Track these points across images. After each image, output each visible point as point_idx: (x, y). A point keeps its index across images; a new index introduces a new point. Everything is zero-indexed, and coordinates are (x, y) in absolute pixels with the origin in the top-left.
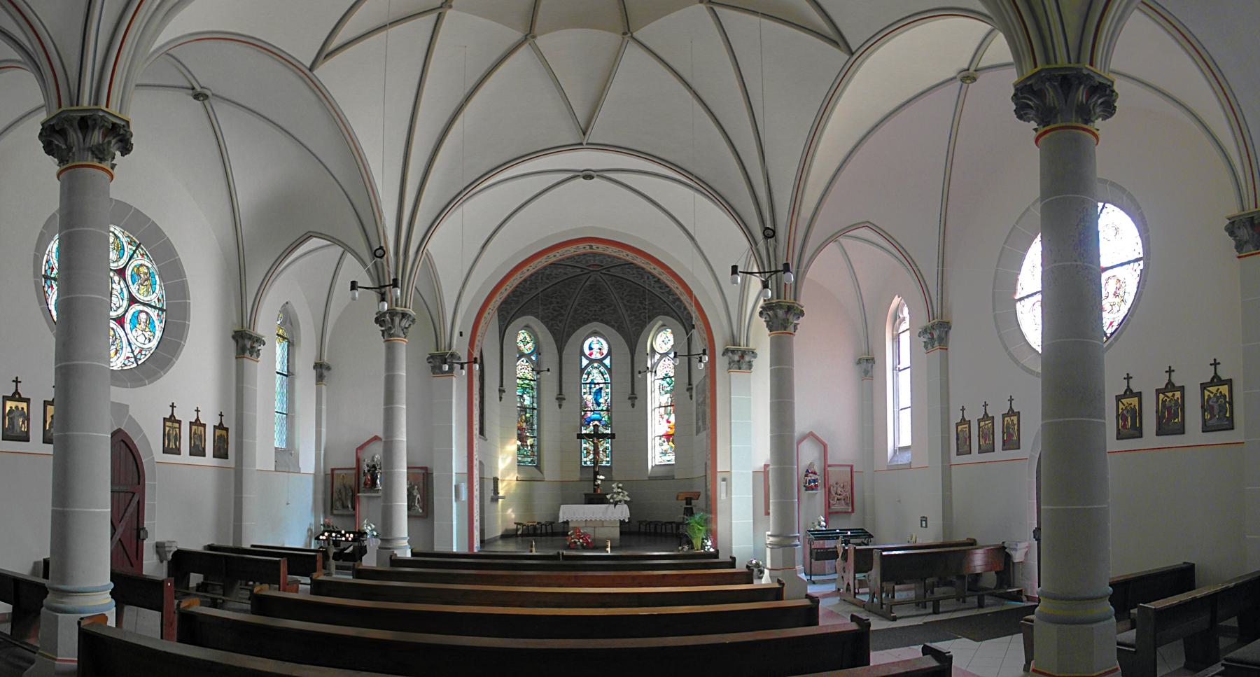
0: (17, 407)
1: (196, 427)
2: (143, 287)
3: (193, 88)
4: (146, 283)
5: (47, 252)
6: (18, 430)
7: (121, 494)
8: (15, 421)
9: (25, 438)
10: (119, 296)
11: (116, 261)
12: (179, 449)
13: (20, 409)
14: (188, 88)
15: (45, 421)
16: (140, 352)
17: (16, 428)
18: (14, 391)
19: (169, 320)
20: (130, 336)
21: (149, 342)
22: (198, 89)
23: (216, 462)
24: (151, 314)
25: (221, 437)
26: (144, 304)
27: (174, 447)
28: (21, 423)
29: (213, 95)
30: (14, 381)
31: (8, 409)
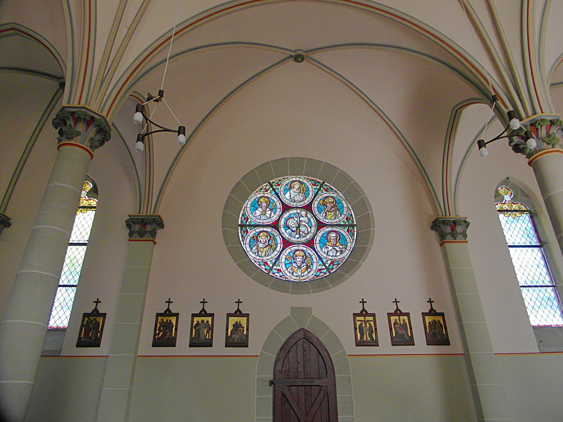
0: (203, 321)
1: (397, 317)
2: (330, 213)
3: (292, 56)
4: (332, 210)
5: (243, 209)
6: (203, 339)
7: (300, 387)
8: (201, 331)
9: (209, 344)
10: (307, 225)
11: (302, 201)
12: (377, 341)
13: (205, 322)
14: (289, 58)
15: (227, 329)
16: (332, 263)
17: (201, 337)
18: (362, 309)
19: (358, 232)
20: (322, 254)
21: (341, 254)
22: (293, 54)
23: (434, 349)
24: (341, 231)
25: (433, 324)
26: (332, 226)
27: (369, 339)
28: (205, 333)
29: (306, 52)
30: (428, 302)
31: (195, 323)
